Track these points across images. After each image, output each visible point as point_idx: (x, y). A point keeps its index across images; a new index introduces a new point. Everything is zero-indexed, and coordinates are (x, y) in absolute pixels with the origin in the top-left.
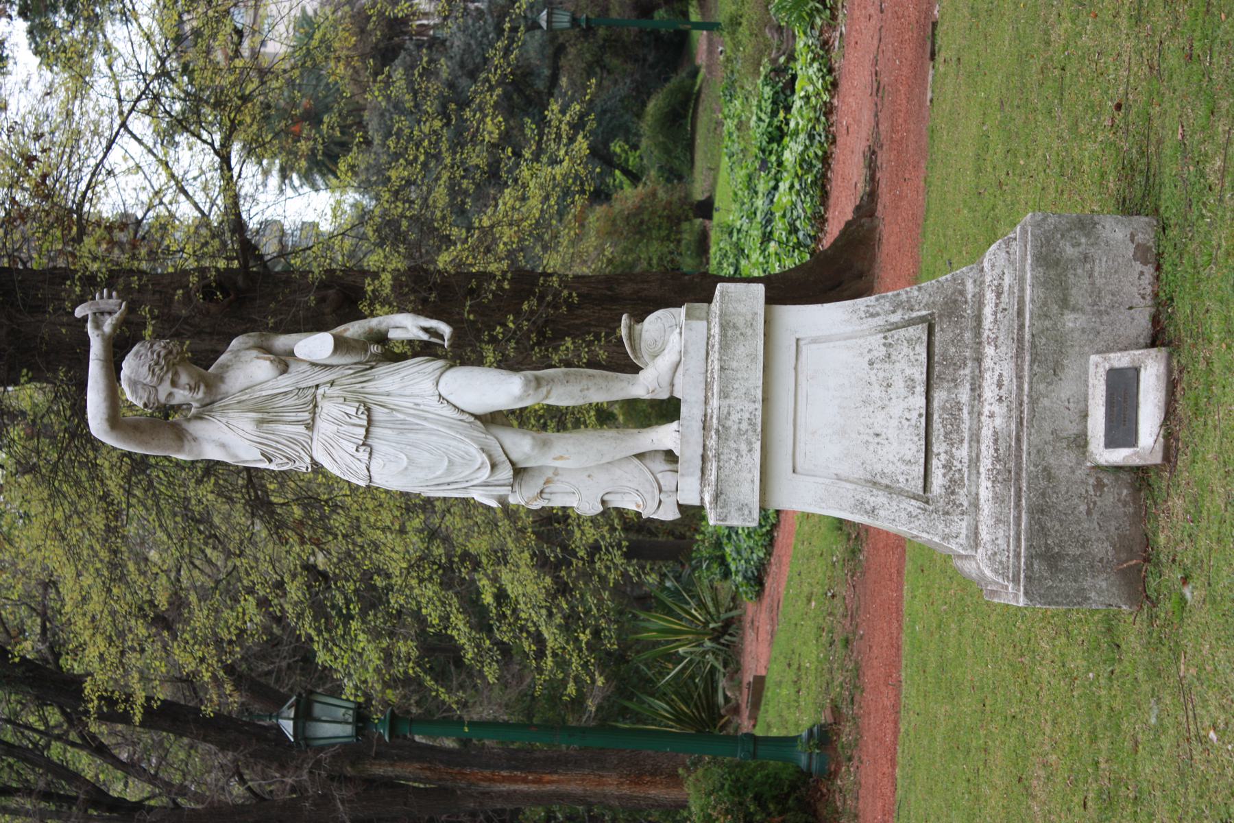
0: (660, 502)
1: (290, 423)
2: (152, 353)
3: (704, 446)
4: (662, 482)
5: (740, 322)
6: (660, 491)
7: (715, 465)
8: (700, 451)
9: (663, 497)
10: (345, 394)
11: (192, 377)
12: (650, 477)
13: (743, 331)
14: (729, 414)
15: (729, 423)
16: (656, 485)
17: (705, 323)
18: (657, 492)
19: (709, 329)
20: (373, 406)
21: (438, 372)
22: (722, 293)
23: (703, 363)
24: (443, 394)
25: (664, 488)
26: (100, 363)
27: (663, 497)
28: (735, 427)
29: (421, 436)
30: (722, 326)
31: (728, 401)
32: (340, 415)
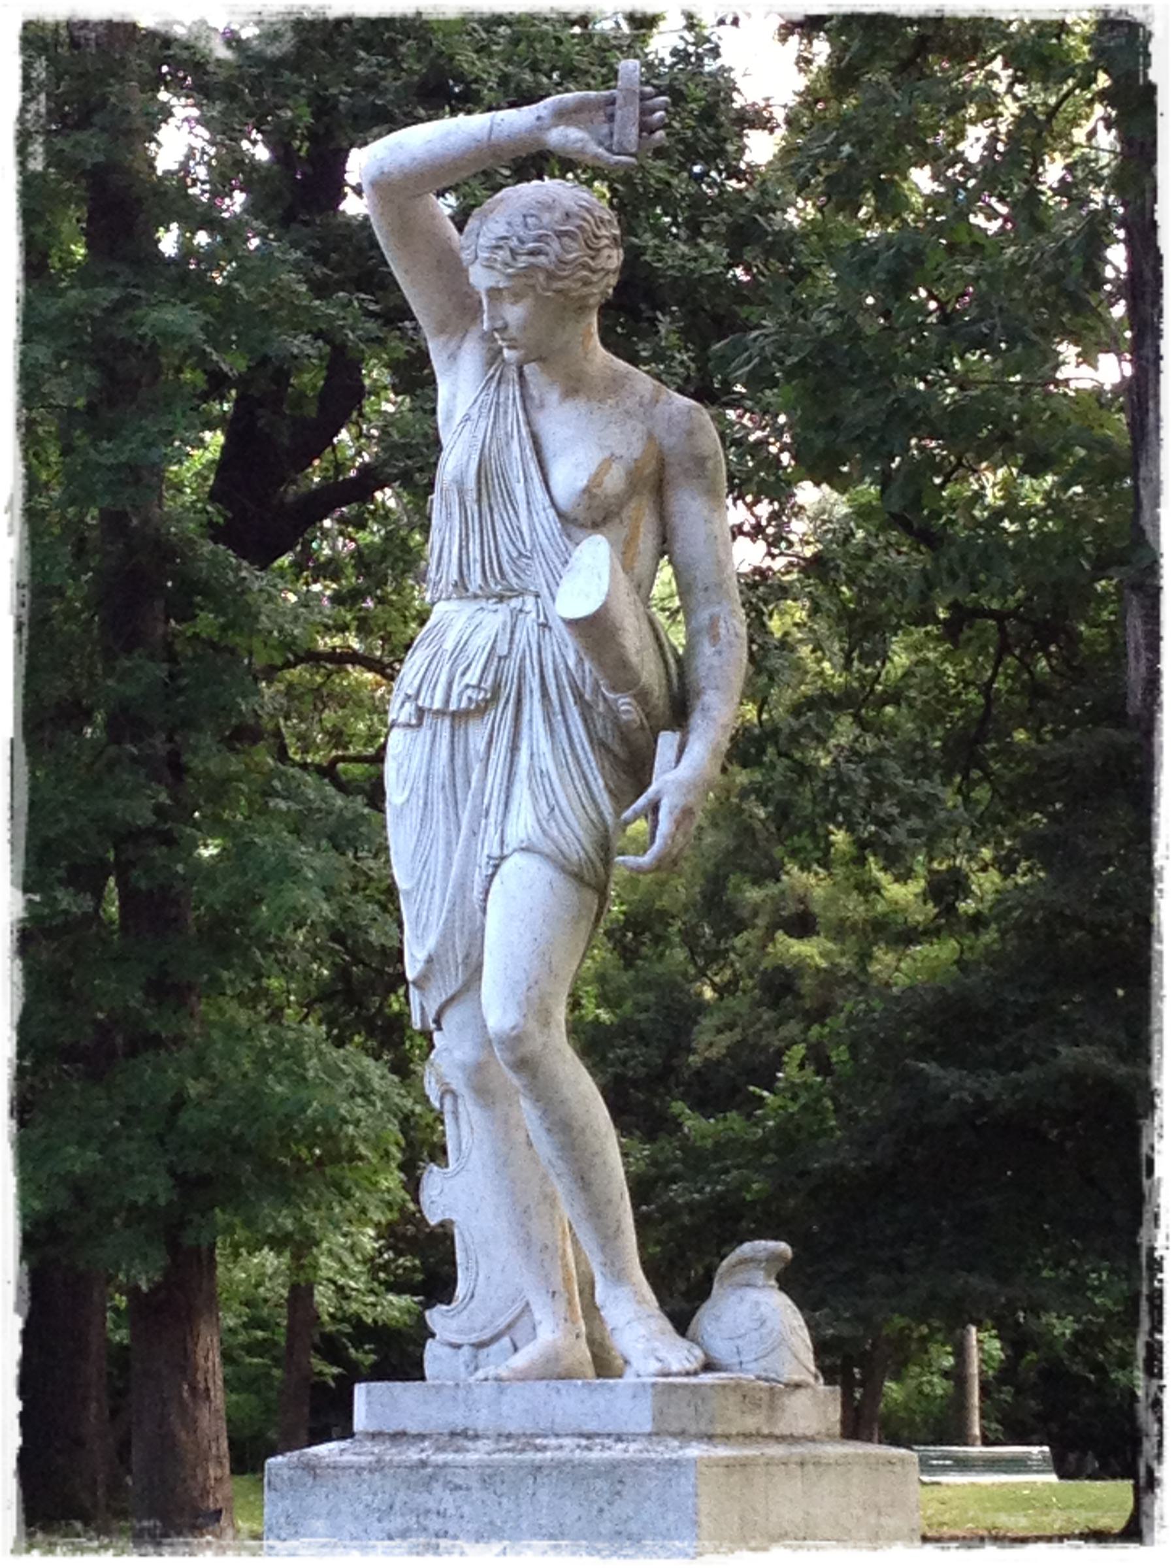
0: (458, 1347)
1: (463, 547)
2: (539, 239)
3: (422, 1437)
4: (495, 1347)
5: (624, 1508)
6: (480, 1345)
7: (364, 1460)
8: (413, 1428)
9: (466, 1350)
10: (516, 656)
11: (523, 328)
12: (502, 1322)
13: (606, 1515)
14: (458, 1488)
15: (437, 1488)
16: (486, 1336)
17: (648, 1428)
18: (474, 1338)
19: (635, 1437)
20: (489, 718)
21: (547, 847)
22: (902, 1460)
23: (574, 1427)
24: (506, 867)
25: (483, 1353)
26: (484, 135)
27: (466, 1350)
28: (432, 1505)
29: (441, 829)
30: (614, 1465)
31: (475, 1484)
32: (471, 649)
